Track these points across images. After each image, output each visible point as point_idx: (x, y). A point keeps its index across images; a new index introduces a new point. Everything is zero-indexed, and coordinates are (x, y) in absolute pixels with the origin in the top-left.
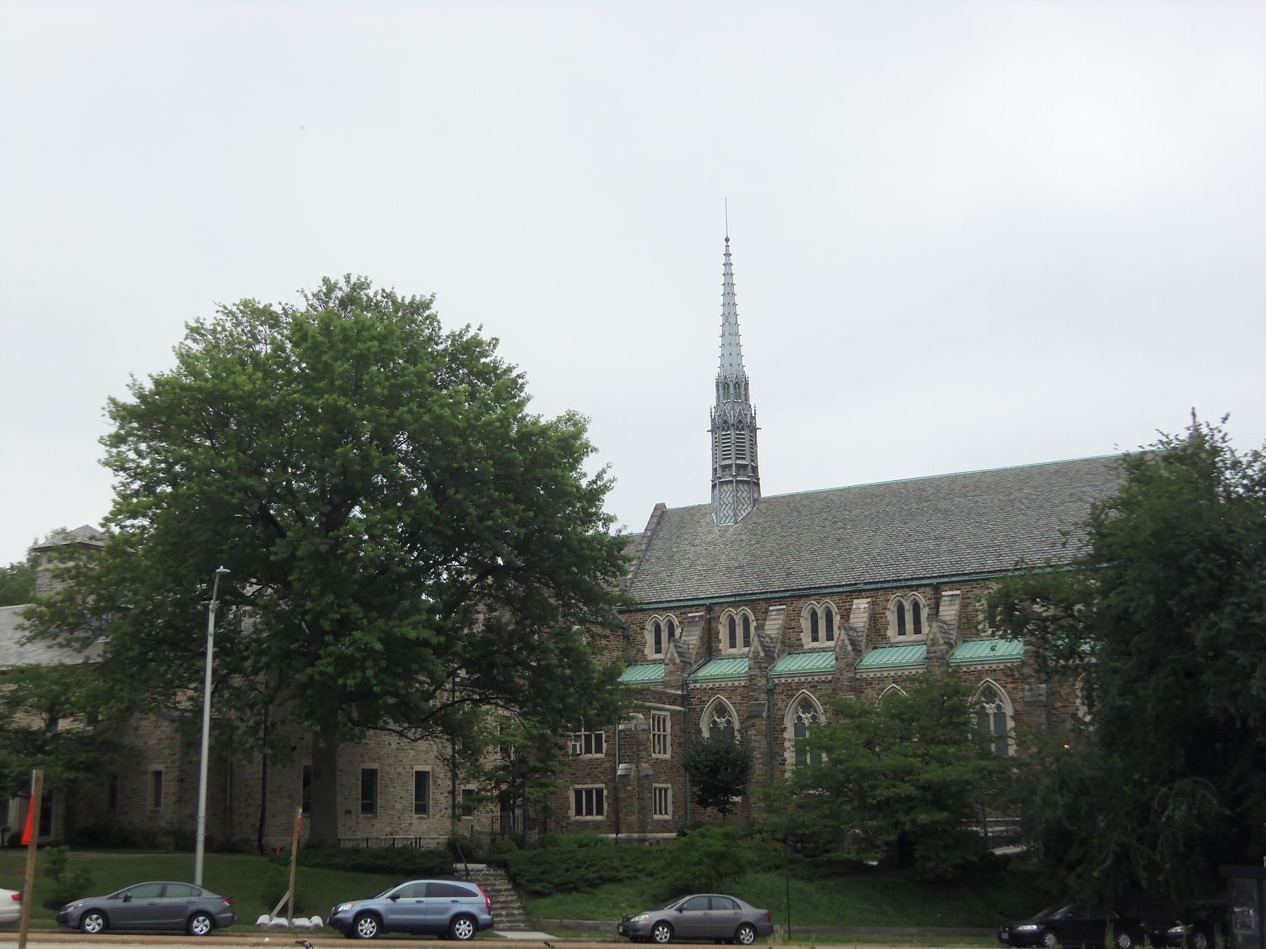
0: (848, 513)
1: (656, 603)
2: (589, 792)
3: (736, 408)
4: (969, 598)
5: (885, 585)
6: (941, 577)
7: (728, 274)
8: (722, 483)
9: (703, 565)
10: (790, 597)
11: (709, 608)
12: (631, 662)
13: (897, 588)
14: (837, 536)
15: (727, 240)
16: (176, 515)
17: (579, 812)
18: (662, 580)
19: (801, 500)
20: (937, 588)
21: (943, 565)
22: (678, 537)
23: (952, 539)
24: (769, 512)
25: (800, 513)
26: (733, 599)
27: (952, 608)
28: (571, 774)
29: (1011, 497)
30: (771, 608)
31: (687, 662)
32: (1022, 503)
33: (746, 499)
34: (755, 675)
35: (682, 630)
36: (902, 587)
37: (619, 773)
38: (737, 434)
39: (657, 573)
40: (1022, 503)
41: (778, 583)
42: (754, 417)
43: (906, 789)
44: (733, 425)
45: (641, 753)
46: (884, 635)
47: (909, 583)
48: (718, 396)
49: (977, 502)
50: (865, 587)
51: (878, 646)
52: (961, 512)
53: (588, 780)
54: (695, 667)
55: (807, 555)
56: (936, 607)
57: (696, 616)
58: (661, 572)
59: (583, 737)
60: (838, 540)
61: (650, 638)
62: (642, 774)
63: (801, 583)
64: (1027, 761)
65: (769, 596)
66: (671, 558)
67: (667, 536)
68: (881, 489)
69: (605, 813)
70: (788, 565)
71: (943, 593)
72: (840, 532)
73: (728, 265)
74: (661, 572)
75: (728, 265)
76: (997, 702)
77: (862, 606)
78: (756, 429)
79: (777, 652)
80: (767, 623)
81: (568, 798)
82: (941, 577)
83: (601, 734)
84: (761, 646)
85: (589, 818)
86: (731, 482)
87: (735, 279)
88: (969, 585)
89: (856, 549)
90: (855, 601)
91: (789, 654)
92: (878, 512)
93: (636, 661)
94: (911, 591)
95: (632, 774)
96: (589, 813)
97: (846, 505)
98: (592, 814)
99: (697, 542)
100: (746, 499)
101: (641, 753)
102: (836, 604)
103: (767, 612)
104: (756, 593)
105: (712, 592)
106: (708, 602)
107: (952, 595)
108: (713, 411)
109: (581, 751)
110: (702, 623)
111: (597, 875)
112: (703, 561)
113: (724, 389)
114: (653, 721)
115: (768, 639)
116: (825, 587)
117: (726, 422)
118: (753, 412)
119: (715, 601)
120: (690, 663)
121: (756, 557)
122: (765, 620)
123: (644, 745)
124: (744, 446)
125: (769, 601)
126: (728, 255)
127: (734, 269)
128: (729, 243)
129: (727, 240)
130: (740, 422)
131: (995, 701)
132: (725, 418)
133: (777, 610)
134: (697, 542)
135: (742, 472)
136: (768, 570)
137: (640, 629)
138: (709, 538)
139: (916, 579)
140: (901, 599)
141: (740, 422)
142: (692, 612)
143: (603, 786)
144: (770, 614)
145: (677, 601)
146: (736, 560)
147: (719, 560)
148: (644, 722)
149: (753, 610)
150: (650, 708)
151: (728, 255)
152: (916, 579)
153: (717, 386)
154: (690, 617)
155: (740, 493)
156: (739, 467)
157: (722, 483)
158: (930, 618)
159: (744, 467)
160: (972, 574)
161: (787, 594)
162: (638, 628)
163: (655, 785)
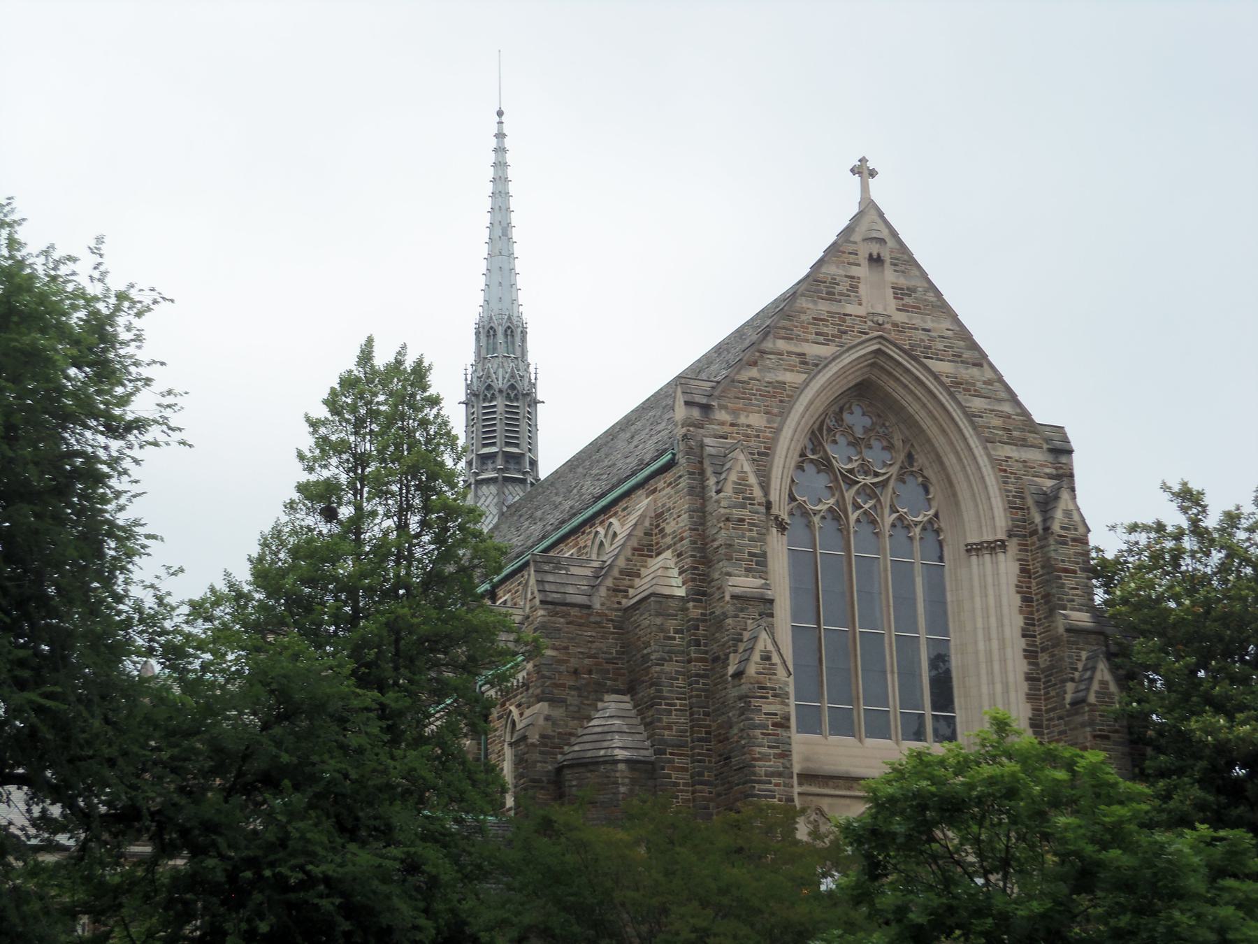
3: (506, 365)
7: (500, 165)
8: (479, 483)
15: (500, 113)
16: (4, 769)
38: (485, 408)
42: (534, 384)
44: (500, 391)
48: (479, 347)
64: (334, 820)
73: (500, 150)
75: (500, 150)
78: (536, 402)
86: (494, 480)
87: (511, 173)
108: (470, 372)
111: (1222, 833)
113: (488, 336)
117: (489, 387)
118: (533, 377)
126: (500, 136)
127: (509, 158)
128: (504, 119)
129: (500, 113)
130: (512, 387)
132: (489, 381)
141: (512, 387)
151: (500, 136)
153: (478, 334)
155: (483, 499)
157: (479, 483)
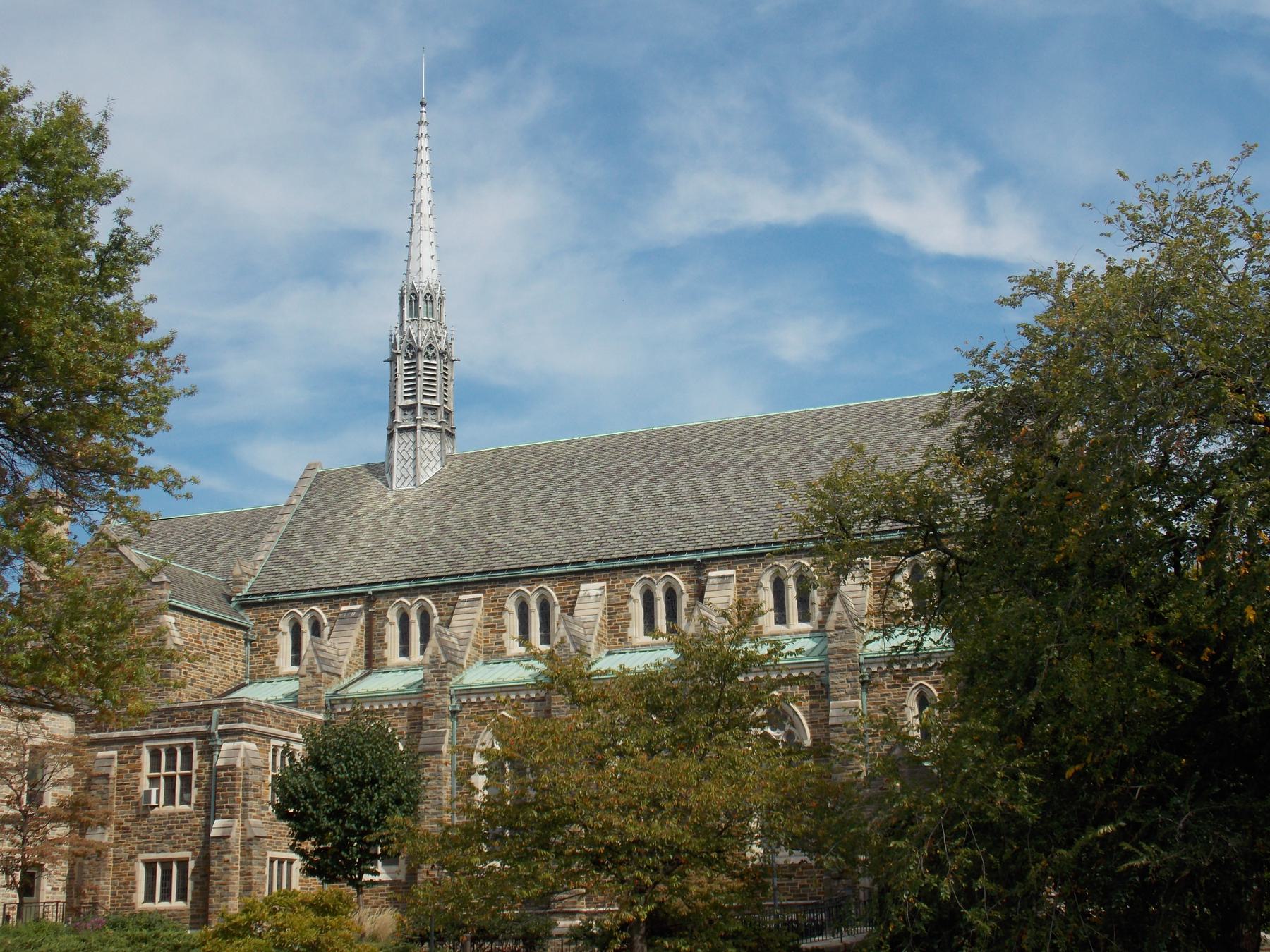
0: (576, 470)
1: (297, 591)
2: (166, 864)
4: (747, 581)
5: (627, 563)
6: (707, 550)
9: (368, 540)
10: (490, 581)
11: (370, 599)
12: (256, 677)
13: (644, 567)
14: (561, 501)
17: (150, 897)
18: (308, 562)
19: (512, 454)
20: (700, 567)
21: (712, 532)
22: (335, 505)
23: (723, 500)
24: (467, 471)
25: (509, 471)
26: (406, 585)
27: (724, 593)
28: (140, 837)
29: (807, 447)
30: (461, 598)
31: (334, 674)
32: (822, 454)
33: (435, 454)
34: (431, 691)
35: (331, 631)
36: (652, 566)
37: (214, 833)
39: (302, 553)
40: (822, 454)
41: (473, 563)
43: (664, 829)
45: (249, 803)
46: (622, 635)
47: (661, 560)
49: (759, 453)
50: (598, 566)
51: (613, 650)
52: (737, 466)
53: (166, 846)
54: (346, 682)
55: (516, 525)
56: (699, 595)
57: (352, 611)
58: (306, 551)
59: (162, 780)
60: (562, 505)
61: (285, 642)
62: (249, 835)
63: (501, 562)
65: (459, 579)
66: (323, 532)
67: (321, 504)
68: (624, 440)
69: (189, 897)
70: (489, 539)
71: (711, 574)
72: (564, 494)
74: (306, 551)
76: (788, 727)
77: (593, 593)
79: (466, 657)
80: (454, 617)
81: (133, 874)
82: (707, 550)
83: (182, 769)
84: (442, 646)
85: (165, 905)
88: (747, 562)
89: (587, 515)
90: (583, 586)
91: (486, 663)
92: (620, 468)
93: (262, 677)
94: (664, 571)
95: (233, 835)
96: (166, 896)
97: (574, 461)
98: (153, 900)
99: (361, 511)
100: (435, 454)
101: (249, 803)
102: (555, 590)
103: (454, 604)
104: (441, 577)
105: (378, 575)
106: (370, 590)
107: (723, 577)
109: (158, 801)
110: (362, 620)
112: (368, 535)
113: (411, 302)
114: (274, 756)
115: (453, 639)
116: (541, 567)
119: (381, 588)
120: (339, 676)
121: (444, 529)
122: (452, 614)
123: (255, 790)
124: (435, 370)
125: (459, 587)
130: (431, 347)
131: (784, 726)
133: (469, 600)
134: (361, 511)
135: (430, 415)
136: (459, 546)
137: (271, 630)
138: (380, 506)
139: (672, 553)
140: (649, 583)
141: (431, 347)
142: (347, 605)
143: (188, 854)
144: (458, 605)
145: (326, 588)
146: (415, 533)
147: (390, 534)
148: (257, 755)
149: (435, 601)
150: (268, 736)
152: (672, 553)
154: (344, 612)
155: (426, 445)
156: (427, 408)
158: (690, 608)
159: (433, 409)
160: (752, 545)
161: (486, 577)
162: (268, 629)
163: (271, 854)
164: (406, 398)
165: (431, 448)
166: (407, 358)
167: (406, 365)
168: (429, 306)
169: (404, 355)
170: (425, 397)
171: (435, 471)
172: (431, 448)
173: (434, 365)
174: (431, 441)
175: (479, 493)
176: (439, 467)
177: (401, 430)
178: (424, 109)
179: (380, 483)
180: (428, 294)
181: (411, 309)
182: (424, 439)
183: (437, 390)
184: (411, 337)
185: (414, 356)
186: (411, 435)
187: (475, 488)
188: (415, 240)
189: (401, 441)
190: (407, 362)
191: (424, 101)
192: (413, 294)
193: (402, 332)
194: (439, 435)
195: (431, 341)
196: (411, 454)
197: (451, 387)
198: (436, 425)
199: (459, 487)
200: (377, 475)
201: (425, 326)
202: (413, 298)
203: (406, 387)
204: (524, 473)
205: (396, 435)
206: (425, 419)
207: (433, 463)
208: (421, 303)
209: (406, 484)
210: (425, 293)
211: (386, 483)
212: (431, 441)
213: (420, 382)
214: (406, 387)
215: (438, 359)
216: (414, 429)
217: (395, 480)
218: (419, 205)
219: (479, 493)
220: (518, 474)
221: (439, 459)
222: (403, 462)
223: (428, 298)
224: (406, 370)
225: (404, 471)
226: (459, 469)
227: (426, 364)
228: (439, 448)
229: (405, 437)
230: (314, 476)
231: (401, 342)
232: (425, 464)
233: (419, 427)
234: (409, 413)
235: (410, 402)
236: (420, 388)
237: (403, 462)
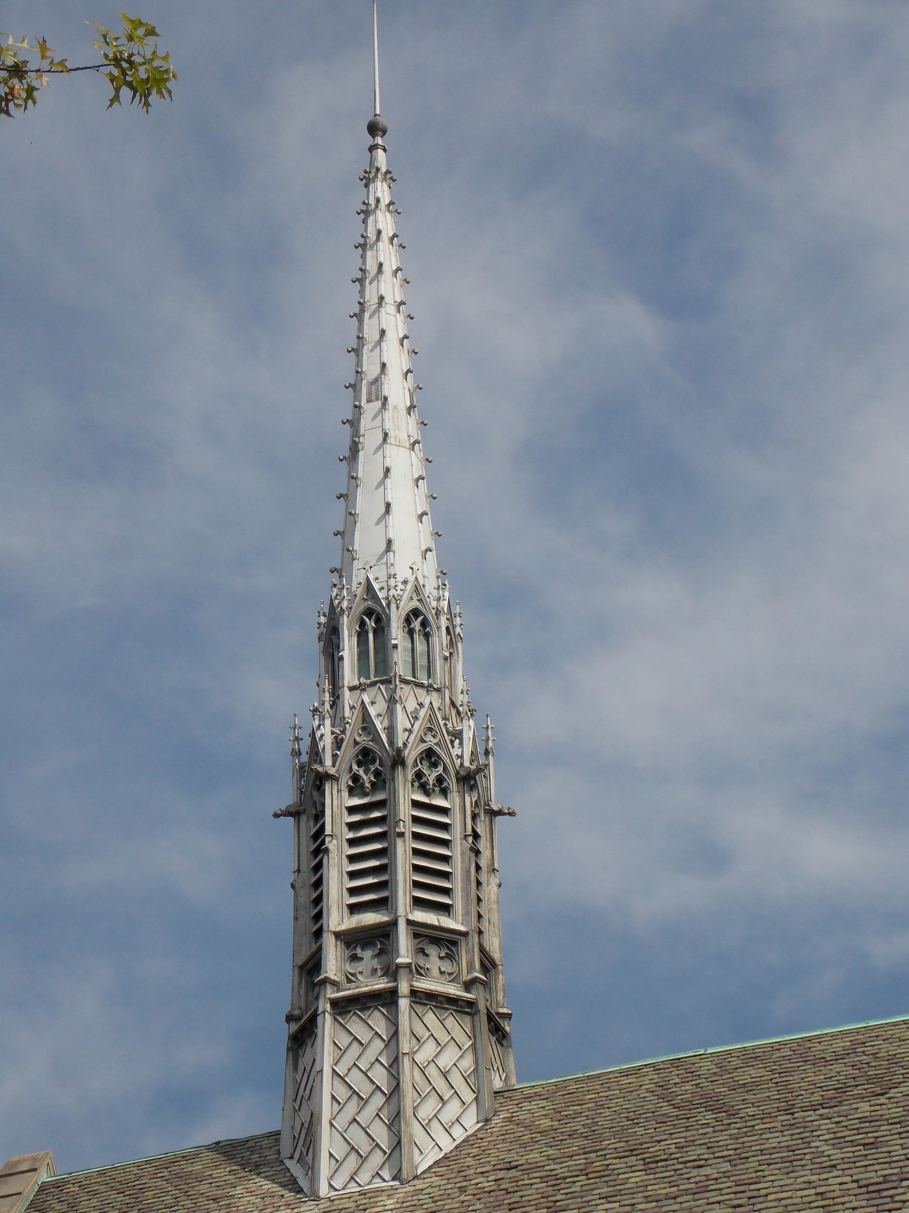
33: (456, 1079)
113: (362, 635)
135: (434, 961)
141: (429, 755)
164: (354, 909)
165: (447, 1059)
166: (356, 787)
167: (352, 810)
168: (420, 646)
169: (345, 780)
170: (418, 903)
171: (459, 1134)
172: (447, 1059)
173: (444, 811)
174: (443, 1038)
175: (637, 1178)
176: (471, 1121)
177: (342, 1007)
178: (379, 140)
179: (268, 1186)
180: (416, 613)
181: (363, 655)
182: (419, 1029)
183: (455, 820)
184: (367, 725)
185: (381, 781)
186: (378, 1020)
187: (619, 1164)
188: (370, 332)
189: (344, 1040)
190: (356, 801)
191: (382, 121)
192: (369, 612)
193: (338, 720)
194: (467, 1021)
195: (431, 741)
196: (380, 1076)
197: (490, 891)
198: (454, 990)
199: (559, 1169)
200: (256, 1168)
201: (409, 698)
202: (371, 624)
203: (353, 875)
204: (789, 1111)
205: (327, 1025)
206: (420, 971)
207: (452, 1109)
208: (397, 633)
209: (364, 1177)
210: (407, 606)
211: (293, 1185)
212: (443, 1038)
213: (403, 850)
214: (353, 875)
215: (455, 796)
216: (388, 998)
217: (325, 1167)
218: (376, 381)
219: (637, 1178)
220: (766, 1116)
221: (469, 1096)
222: (352, 1108)
223: (416, 624)
224: (352, 826)
225: (357, 1136)
226: (545, 1123)
227: (416, 804)
228: (467, 1063)
229: (356, 1027)
230: (30, 1193)
231: (338, 743)
232: (428, 1109)
233: (404, 988)
234: (367, 954)
235: (370, 918)
236: (403, 876)
237: (352, 1162)
